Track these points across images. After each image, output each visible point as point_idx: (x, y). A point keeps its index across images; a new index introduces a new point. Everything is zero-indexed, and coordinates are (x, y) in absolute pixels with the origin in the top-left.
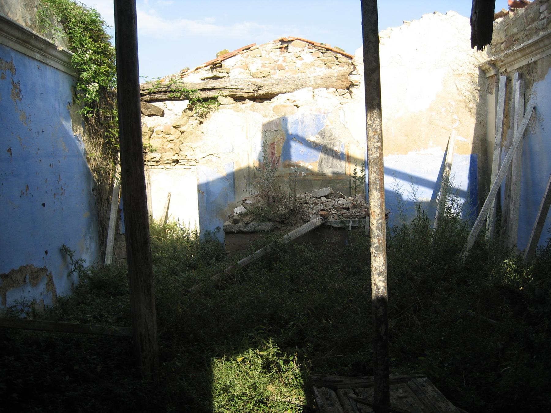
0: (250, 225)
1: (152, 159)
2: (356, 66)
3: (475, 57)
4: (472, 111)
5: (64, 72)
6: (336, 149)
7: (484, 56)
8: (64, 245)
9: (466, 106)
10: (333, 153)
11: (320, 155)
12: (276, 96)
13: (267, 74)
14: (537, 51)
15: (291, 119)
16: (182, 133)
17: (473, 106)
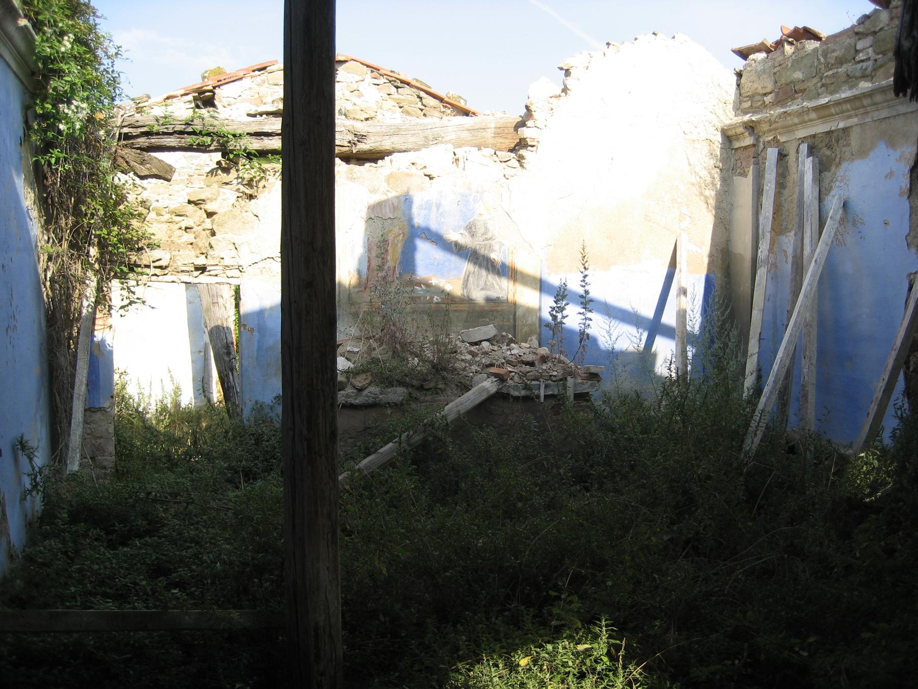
0: (366, 392)
1: (154, 262)
2: (533, 113)
3: (715, 114)
4: (709, 202)
5: (15, 73)
6: (493, 256)
7: (728, 113)
8: (25, 438)
9: (701, 194)
10: (487, 264)
11: (467, 267)
12: (388, 156)
13: (373, 114)
14: (853, 112)
15: (418, 200)
16: (210, 215)
17: (711, 193)
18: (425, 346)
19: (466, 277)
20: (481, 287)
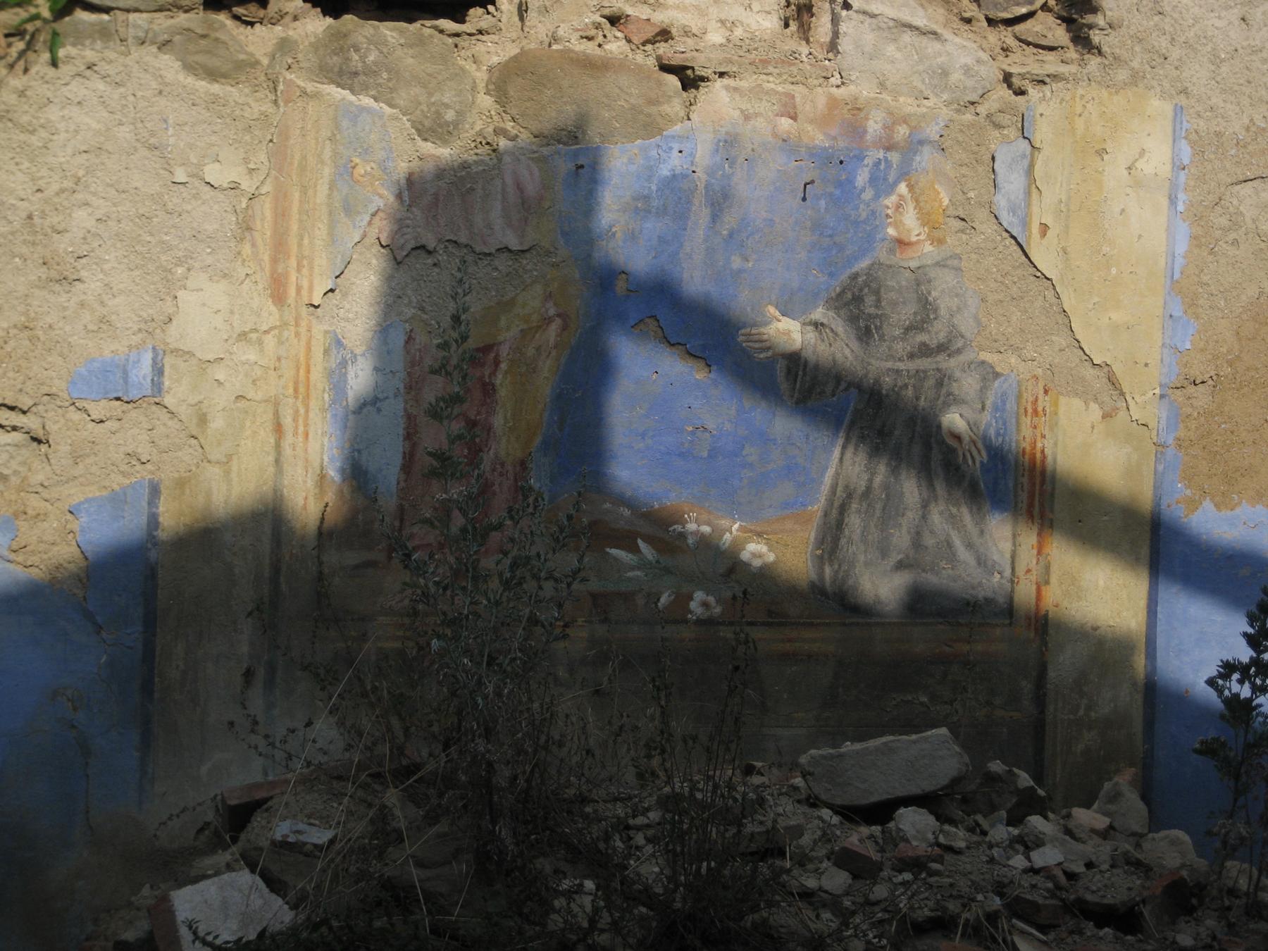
6: (954, 420)
18: (640, 820)
19: (834, 513)
20: (895, 557)
